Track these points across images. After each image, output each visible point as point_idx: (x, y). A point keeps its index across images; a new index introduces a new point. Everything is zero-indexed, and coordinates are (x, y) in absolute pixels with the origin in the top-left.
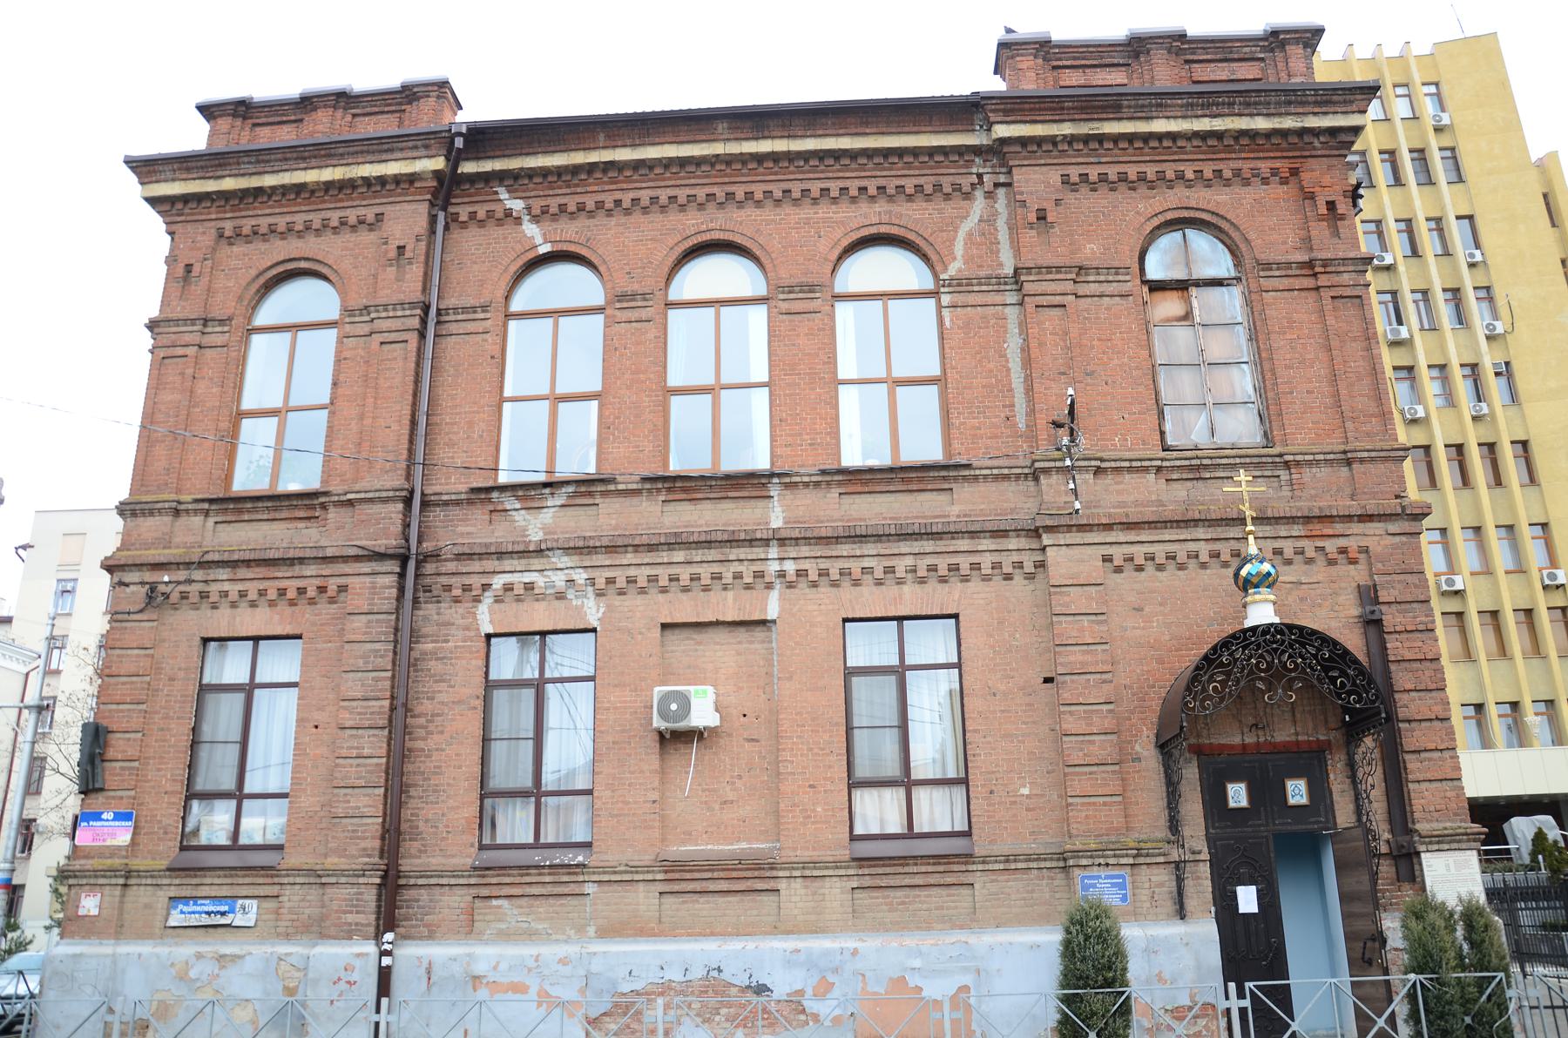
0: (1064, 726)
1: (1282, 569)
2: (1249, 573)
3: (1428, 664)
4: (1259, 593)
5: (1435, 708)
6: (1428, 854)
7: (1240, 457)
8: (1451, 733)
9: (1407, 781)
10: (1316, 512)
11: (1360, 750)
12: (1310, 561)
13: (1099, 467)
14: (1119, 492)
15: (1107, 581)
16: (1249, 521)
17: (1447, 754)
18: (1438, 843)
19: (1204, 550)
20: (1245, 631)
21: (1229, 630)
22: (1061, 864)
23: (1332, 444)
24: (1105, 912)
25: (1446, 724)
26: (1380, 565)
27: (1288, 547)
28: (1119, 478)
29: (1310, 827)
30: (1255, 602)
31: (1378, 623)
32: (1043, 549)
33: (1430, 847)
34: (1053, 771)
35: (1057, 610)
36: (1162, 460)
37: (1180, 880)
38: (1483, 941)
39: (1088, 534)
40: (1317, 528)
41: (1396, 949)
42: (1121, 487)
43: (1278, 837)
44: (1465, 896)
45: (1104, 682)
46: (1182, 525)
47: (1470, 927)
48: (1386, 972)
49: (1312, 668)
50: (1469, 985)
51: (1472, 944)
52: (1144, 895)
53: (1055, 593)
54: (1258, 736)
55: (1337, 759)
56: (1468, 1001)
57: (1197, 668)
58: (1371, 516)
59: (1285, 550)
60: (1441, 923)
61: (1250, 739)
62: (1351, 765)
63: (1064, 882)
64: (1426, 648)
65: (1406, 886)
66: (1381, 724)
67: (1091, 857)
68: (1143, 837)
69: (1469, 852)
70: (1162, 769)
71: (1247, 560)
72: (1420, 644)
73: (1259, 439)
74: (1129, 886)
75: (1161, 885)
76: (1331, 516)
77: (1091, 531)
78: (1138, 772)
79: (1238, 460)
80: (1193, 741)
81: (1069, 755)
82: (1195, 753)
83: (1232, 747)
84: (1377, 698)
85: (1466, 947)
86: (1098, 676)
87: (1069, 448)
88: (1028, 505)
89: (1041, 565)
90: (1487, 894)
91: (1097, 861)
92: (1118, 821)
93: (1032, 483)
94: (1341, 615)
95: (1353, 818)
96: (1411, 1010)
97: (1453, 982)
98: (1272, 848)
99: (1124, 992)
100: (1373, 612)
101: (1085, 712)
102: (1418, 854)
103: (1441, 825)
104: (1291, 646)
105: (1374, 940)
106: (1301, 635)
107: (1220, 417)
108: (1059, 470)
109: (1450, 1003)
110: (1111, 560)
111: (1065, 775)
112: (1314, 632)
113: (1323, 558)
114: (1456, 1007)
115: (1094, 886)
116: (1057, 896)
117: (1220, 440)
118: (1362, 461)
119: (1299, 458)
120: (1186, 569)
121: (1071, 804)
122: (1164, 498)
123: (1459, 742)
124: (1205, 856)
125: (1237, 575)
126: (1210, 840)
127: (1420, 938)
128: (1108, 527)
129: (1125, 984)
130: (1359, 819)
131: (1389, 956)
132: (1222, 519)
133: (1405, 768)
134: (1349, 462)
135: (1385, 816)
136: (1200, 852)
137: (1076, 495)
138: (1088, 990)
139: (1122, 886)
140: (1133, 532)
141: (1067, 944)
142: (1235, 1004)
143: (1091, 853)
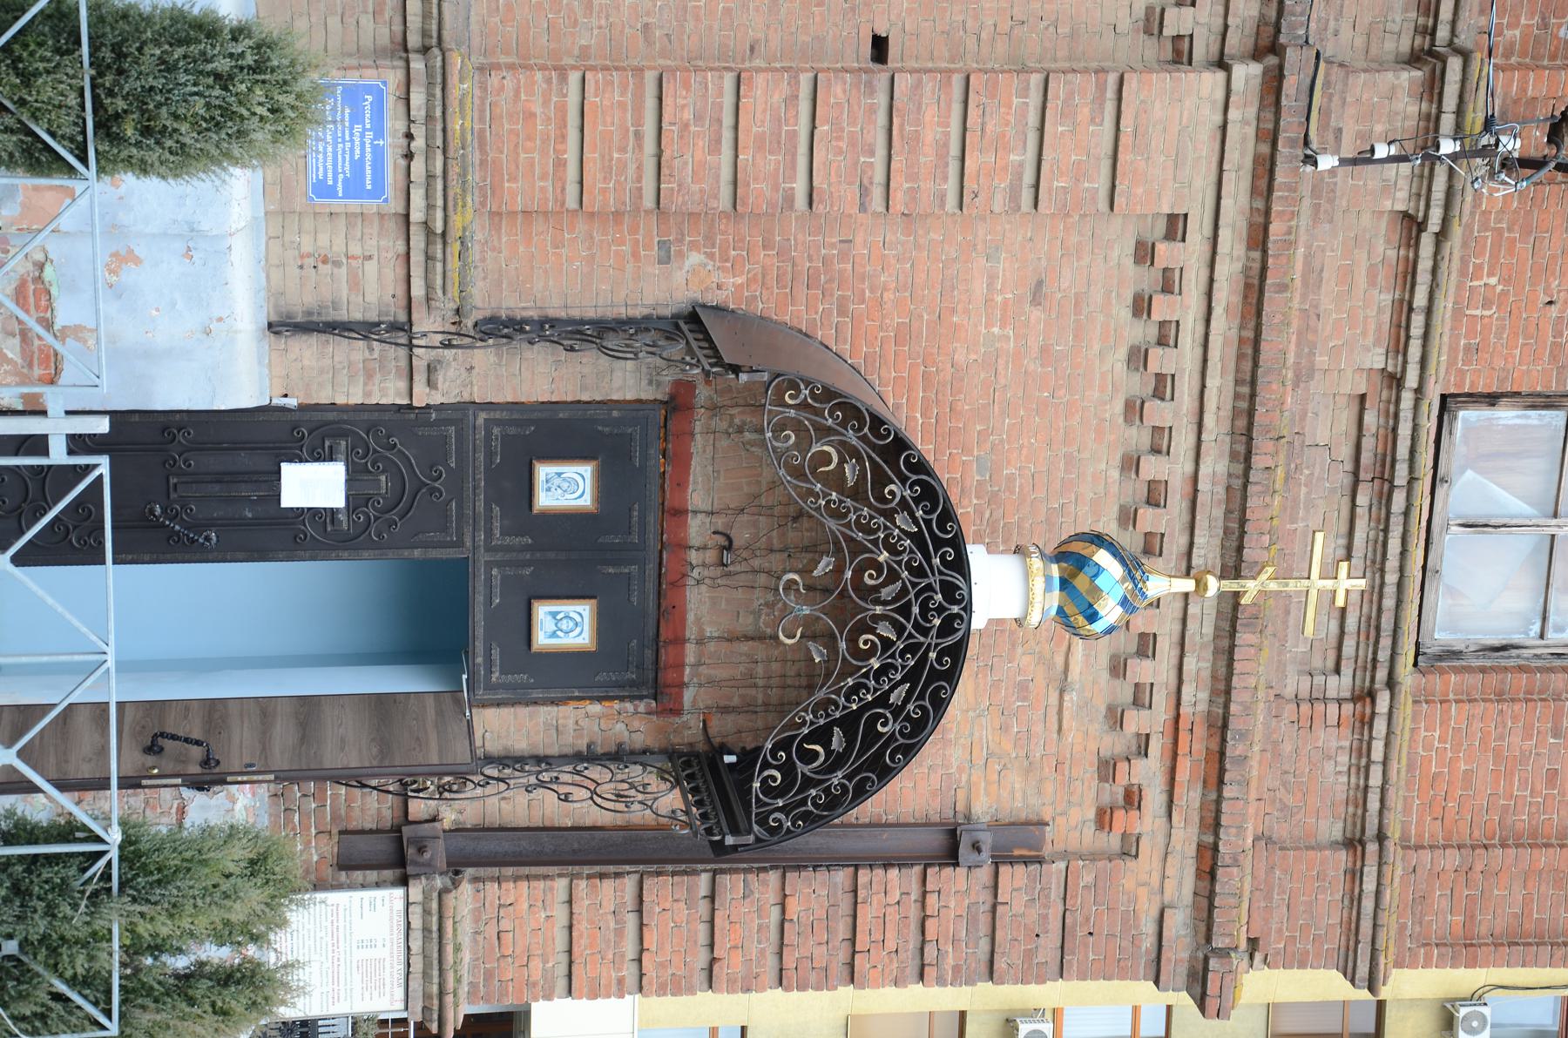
0: (760, 79)
1: (1104, 649)
2: (1099, 570)
3: (842, 955)
4: (1048, 588)
5: (737, 959)
6: (399, 905)
7: (1400, 585)
8: (676, 986)
9: (573, 877)
10: (1234, 749)
11: (652, 780)
12: (1116, 718)
13: (1421, 226)
14: (1346, 275)
15: (1117, 222)
16: (1230, 586)
17: (630, 971)
18: (426, 930)
19: (1172, 469)
20: (958, 544)
21: (966, 509)
22: (414, 40)
23: (1407, 810)
24: (289, 133)
25: (700, 978)
26: (1088, 878)
27: (1156, 671)
28: (1384, 276)
29: (480, 646)
30: (1027, 574)
31: (951, 856)
32: (1222, 64)
33: (416, 912)
34: (649, 41)
35: (1058, 88)
36: (1419, 391)
37: (365, 330)
38: (191, 1001)
39: (1245, 184)
40: (1196, 745)
41: (182, 811)
42: (1361, 279)
43: (460, 573)
44: (297, 977)
45: (864, 191)
46: (1242, 423)
47: (227, 978)
48: (130, 783)
49: (855, 689)
50: (91, 958)
51: (186, 979)
52: (332, 240)
53: (1101, 88)
54: (704, 548)
55: (636, 724)
56: (54, 951)
57: (877, 422)
58: (1213, 876)
59: (1147, 664)
60: (238, 913)
61: (697, 529)
62: (618, 756)
63: (367, 42)
64: (879, 955)
65: (329, 848)
66: (709, 831)
67: (429, 118)
68: (475, 253)
69: (399, 993)
70: (638, 313)
71: (1133, 568)
72: (891, 944)
73: (1441, 635)
74: (354, 205)
75: (355, 283)
76: (1221, 782)
77: (1254, 191)
78: (635, 255)
79: (1391, 578)
80: (703, 393)
81: (686, 85)
82: (673, 397)
83: (682, 484)
84: (773, 831)
85: (181, 963)
86: (879, 176)
87: (1484, 152)
88: (1346, 33)
89: (1180, 54)
90: (304, 1023)
91: (419, 131)
92: (517, 194)
93: (1405, 46)
94: (977, 775)
95: (494, 747)
96: (35, 826)
97: (98, 924)
98: (434, 554)
99: (84, 160)
100: (976, 847)
101: (793, 135)
102: (404, 881)
103: (466, 940)
104: (912, 648)
105: (206, 762)
106: (935, 675)
107: (1517, 549)
108: (1431, 123)
109: (50, 912)
110: (1170, 235)
111: (638, 71)
112: (940, 705)
113: (1120, 749)
114: (42, 925)
115: (357, 118)
116: (334, 22)
117: (1454, 548)
118: (1355, 875)
119: (1380, 726)
120: (1128, 420)
121: (563, 79)
122: (1317, 386)
123: (654, 1001)
124: (422, 396)
125: (1098, 540)
126: (459, 413)
127: (204, 863)
128: (1259, 237)
129: (106, 166)
130: (489, 759)
131: (166, 794)
132: (1243, 521)
133: (602, 876)
134: (1354, 843)
135: (494, 819)
136: (430, 383)
137: (1354, 162)
138: (88, 72)
139: (354, 187)
140: (1237, 299)
141: (207, 28)
142: (56, 429)
143: (439, 117)
